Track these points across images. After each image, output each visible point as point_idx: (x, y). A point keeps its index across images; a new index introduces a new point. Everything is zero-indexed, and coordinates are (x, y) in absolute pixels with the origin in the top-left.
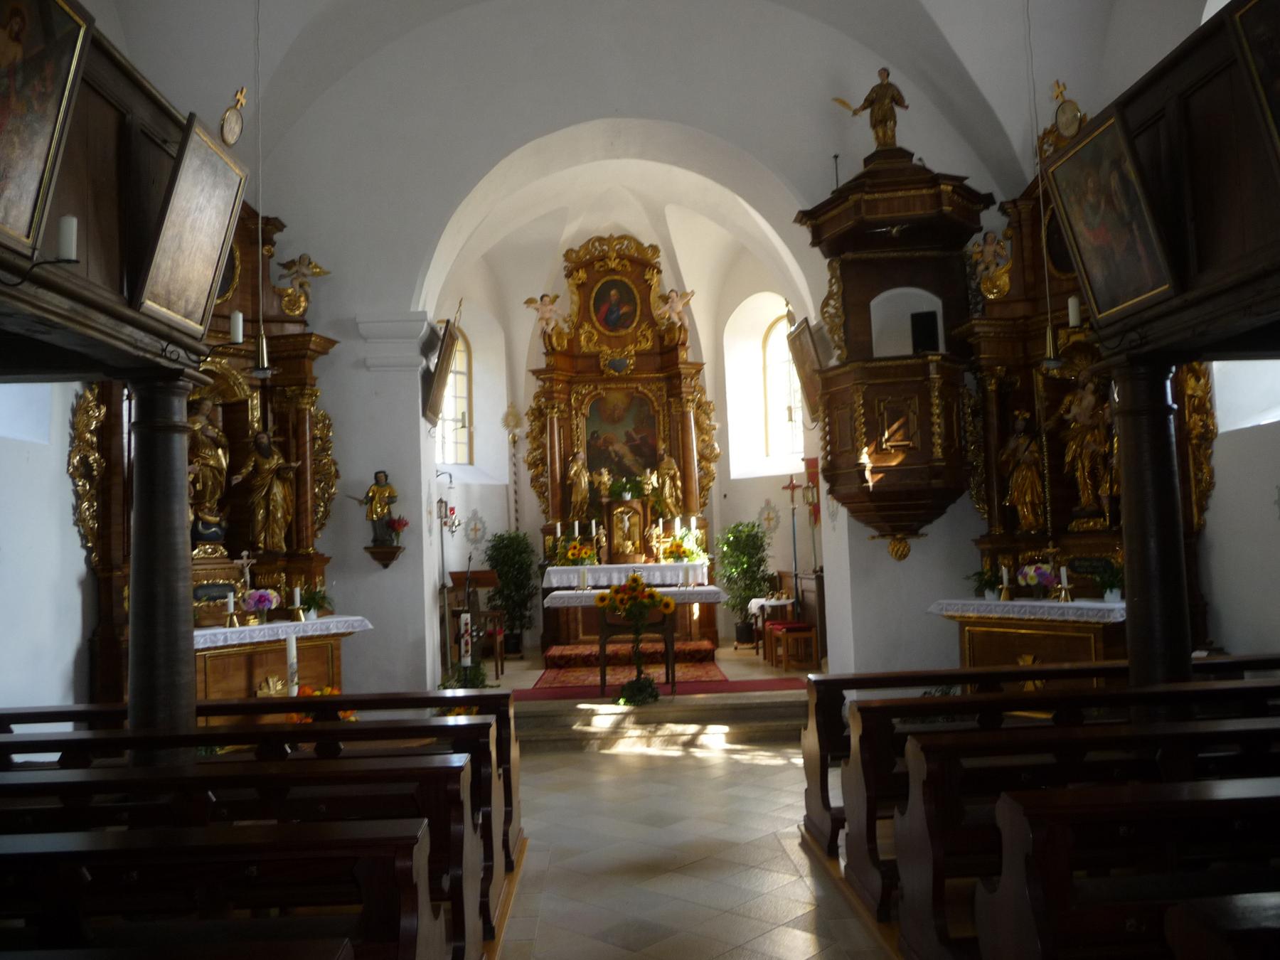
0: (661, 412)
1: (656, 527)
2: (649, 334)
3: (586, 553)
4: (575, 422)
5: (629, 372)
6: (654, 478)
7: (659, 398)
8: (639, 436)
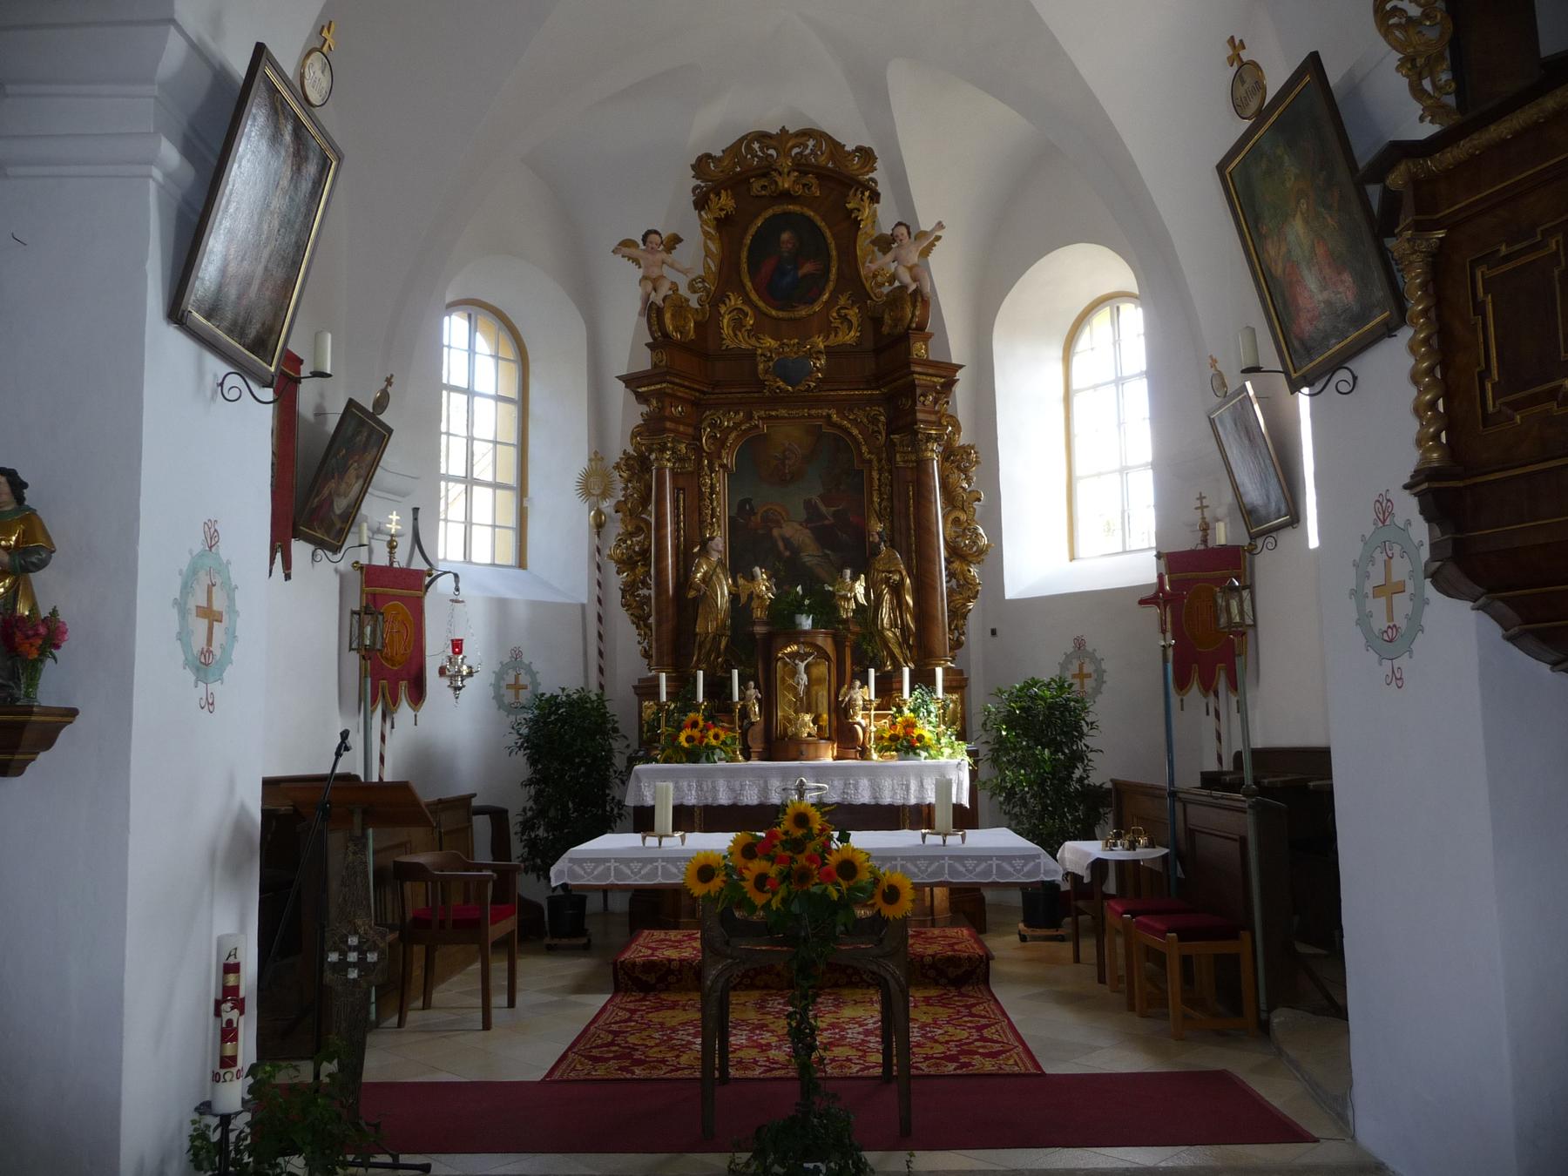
2: (853, 314)
6: (860, 588)
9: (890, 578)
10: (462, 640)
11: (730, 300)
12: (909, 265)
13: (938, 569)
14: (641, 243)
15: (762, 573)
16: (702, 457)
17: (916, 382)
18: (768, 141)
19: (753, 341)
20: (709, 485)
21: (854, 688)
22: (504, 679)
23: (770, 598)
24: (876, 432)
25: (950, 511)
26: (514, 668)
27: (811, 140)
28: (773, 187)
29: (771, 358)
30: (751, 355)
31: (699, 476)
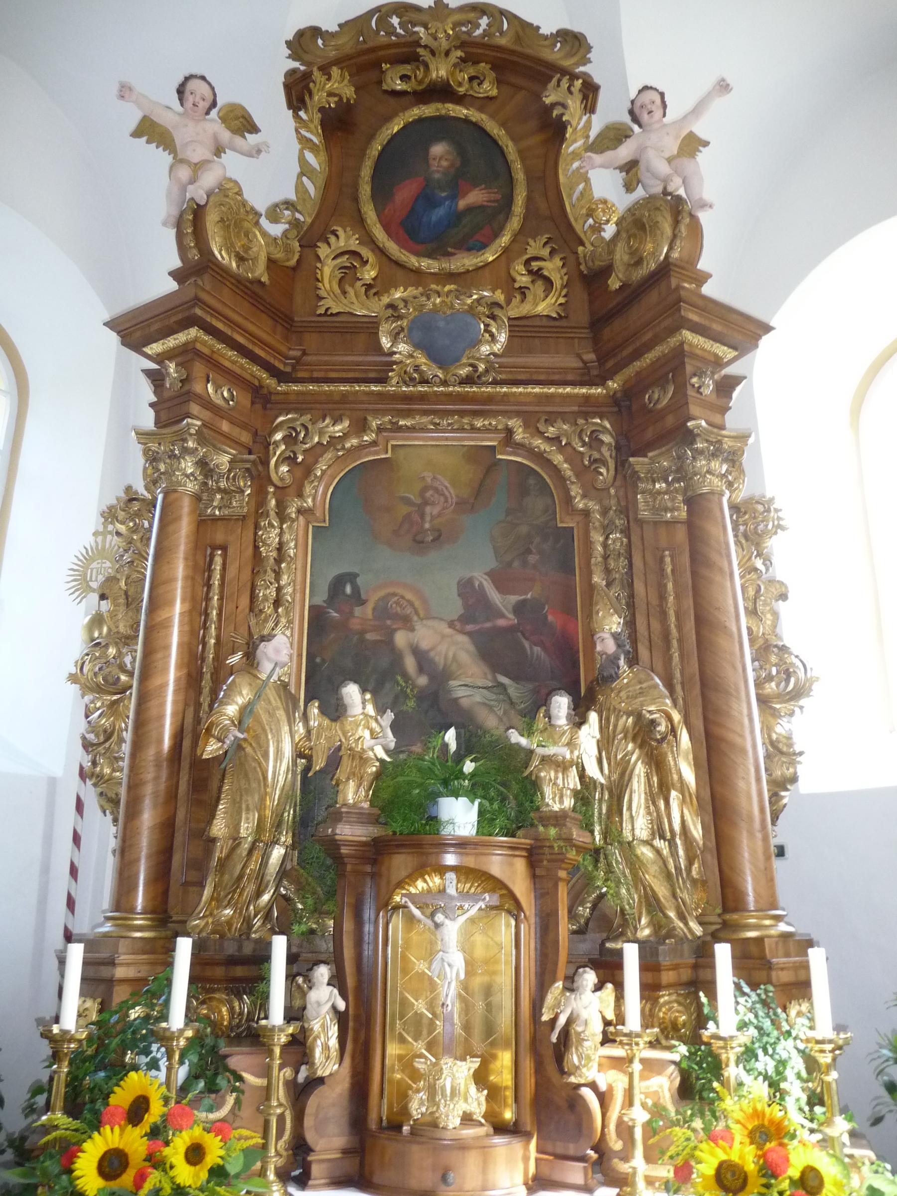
2: (553, 268)
3: (195, 1154)
8: (514, 599)
11: (337, 236)
13: (745, 711)
15: (364, 702)
18: (414, 16)
24: (596, 461)
27: (485, 18)
28: (420, 74)
31: (257, 527)
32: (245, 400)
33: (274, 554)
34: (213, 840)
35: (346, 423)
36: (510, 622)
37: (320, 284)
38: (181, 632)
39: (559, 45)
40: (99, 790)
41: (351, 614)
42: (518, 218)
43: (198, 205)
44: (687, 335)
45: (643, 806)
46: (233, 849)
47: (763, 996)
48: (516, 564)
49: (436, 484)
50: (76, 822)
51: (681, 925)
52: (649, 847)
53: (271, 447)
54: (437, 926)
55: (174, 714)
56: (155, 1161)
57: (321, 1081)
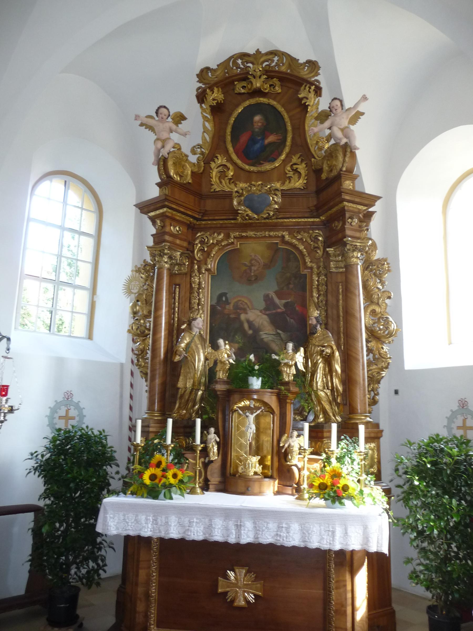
0: (315, 270)
1: (299, 436)
2: (302, 168)
3: (175, 476)
4: (197, 280)
5: (272, 213)
6: (300, 357)
7: (312, 251)
8: (284, 301)
9: (323, 351)
10: (8, 386)
11: (218, 159)
12: (342, 127)
13: (360, 346)
14: (155, 115)
15: (225, 344)
16: (194, 263)
17: (346, 208)
18: (247, 58)
19: (232, 186)
20: (197, 283)
21: (291, 437)
22: (57, 413)
23: (230, 363)
24: (316, 247)
25: (369, 305)
26: (66, 405)
28: (249, 86)
29: (242, 195)
30: (228, 196)
31: (191, 277)
32: (184, 229)
33: (197, 286)
34: (179, 388)
35: (222, 235)
36: (283, 310)
37: (212, 179)
38: (165, 319)
39: (306, 68)
40: (140, 370)
41: (225, 308)
42: (288, 147)
43: (165, 158)
44: (346, 203)
45: (321, 378)
46: (185, 391)
47: (354, 441)
48: (285, 288)
49: (256, 258)
50: (131, 379)
51: (334, 418)
52: (323, 392)
53: (195, 246)
54: (247, 416)
55: (164, 347)
56: (164, 476)
57: (212, 461)
